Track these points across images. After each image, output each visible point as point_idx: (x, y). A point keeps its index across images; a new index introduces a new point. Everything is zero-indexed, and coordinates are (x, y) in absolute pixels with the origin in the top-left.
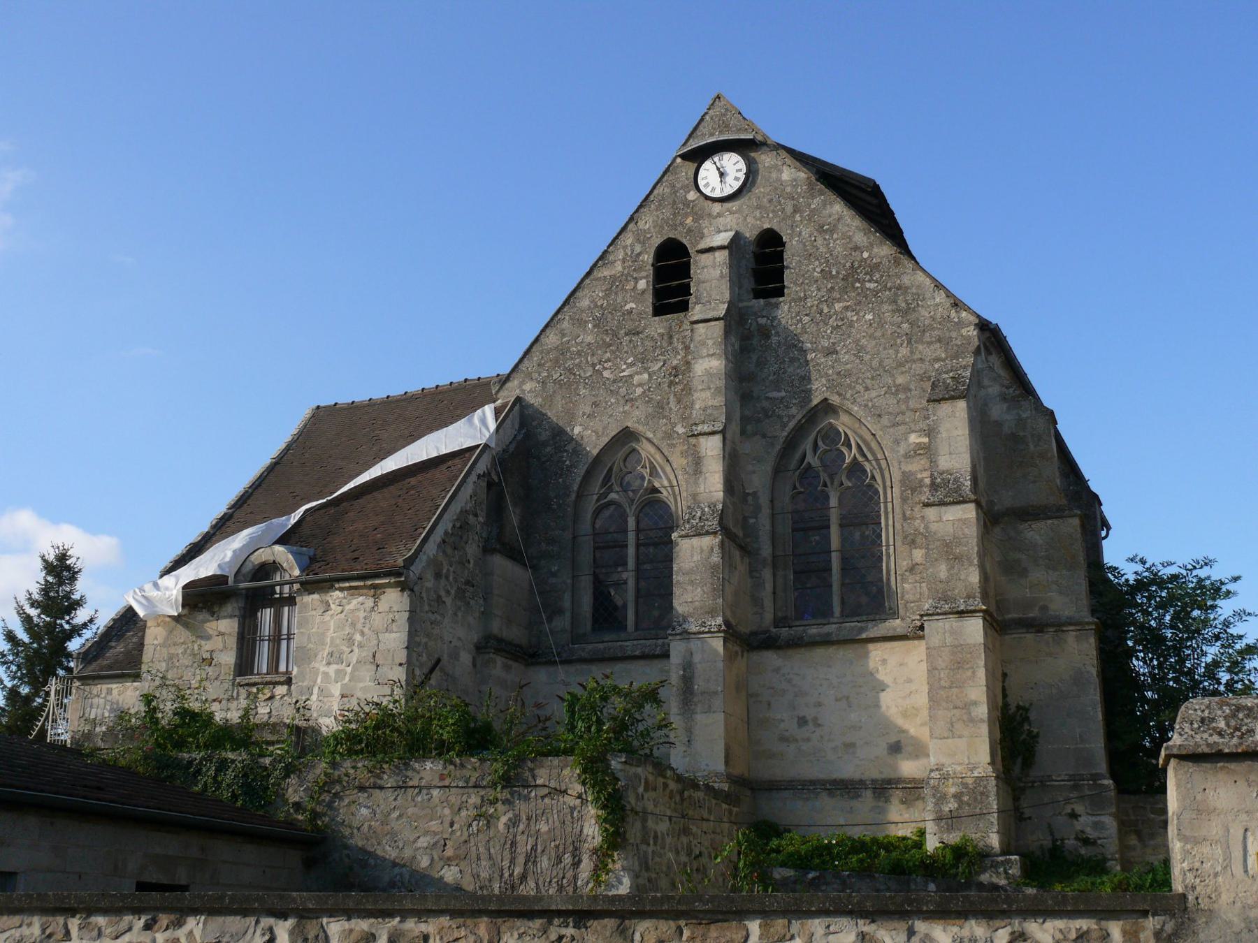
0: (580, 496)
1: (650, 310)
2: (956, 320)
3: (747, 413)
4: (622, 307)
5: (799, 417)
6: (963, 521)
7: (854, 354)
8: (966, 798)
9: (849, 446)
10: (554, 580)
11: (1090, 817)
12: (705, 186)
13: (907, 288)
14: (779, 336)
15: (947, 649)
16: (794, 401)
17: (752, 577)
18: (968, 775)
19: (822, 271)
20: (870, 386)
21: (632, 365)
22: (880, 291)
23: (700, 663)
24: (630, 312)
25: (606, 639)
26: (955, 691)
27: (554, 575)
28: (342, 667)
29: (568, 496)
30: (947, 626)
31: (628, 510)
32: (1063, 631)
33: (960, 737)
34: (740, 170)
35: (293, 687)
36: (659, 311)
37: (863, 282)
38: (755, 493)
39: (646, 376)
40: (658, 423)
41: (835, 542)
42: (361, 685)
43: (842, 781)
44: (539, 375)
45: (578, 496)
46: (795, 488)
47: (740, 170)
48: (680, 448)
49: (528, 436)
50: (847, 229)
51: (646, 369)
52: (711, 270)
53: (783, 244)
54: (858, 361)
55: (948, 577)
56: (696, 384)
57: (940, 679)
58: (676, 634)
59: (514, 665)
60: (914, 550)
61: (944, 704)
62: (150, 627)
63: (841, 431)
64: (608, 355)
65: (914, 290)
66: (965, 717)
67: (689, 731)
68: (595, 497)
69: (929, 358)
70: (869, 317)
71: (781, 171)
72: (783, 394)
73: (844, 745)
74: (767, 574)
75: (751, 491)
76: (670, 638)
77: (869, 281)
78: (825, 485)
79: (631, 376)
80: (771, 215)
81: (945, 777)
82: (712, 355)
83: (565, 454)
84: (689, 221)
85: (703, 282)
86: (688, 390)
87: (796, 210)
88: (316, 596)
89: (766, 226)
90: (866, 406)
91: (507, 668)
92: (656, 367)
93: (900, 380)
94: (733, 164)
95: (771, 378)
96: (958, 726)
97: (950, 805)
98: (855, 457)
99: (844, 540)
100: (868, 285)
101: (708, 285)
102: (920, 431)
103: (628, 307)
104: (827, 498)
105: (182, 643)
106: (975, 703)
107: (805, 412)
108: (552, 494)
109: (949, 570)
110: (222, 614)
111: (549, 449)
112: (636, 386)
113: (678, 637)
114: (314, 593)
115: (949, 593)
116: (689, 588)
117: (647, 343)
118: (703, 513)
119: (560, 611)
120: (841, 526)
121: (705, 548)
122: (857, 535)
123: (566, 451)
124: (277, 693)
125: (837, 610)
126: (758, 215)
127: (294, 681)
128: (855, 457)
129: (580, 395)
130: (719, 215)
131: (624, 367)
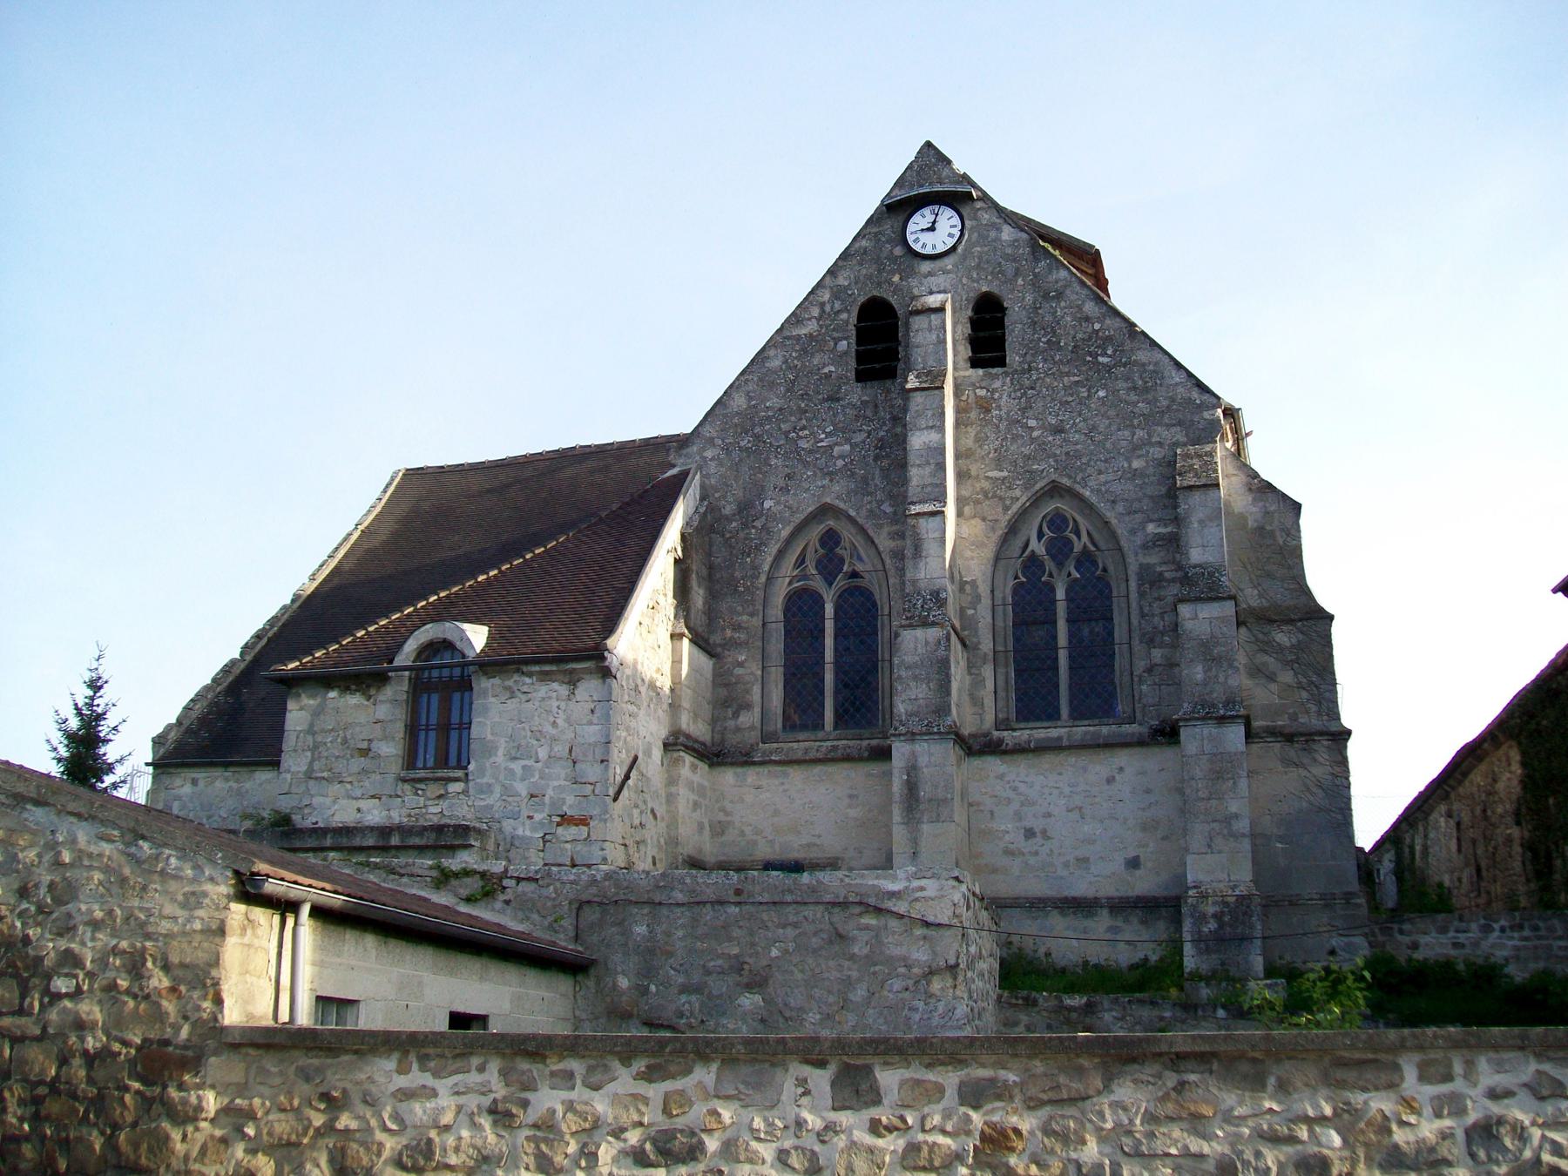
0: (770, 579)
1: (852, 375)
2: (1198, 402)
3: (964, 493)
4: (819, 369)
5: (1024, 499)
6: (1223, 619)
7: (1086, 434)
8: (1226, 919)
9: (1078, 535)
10: (739, 671)
11: (1342, 938)
12: (914, 241)
13: (1144, 365)
14: (1000, 410)
15: (1205, 757)
16: (1018, 483)
17: (970, 673)
18: (1230, 892)
19: (1049, 340)
20: (1103, 469)
21: (828, 435)
22: (1115, 366)
23: (926, 766)
24: (828, 376)
25: (800, 739)
26: (1214, 802)
27: (741, 665)
28: (530, 763)
29: (758, 578)
30: (1206, 731)
31: (825, 597)
32: (1314, 740)
33: (1220, 852)
34: (955, 226)
35: (471, 784)
36: (861, 377)
37: (1095, 356)
38: (974, 582)
39: (847, 447)
40: (862, 500)
41: (1062, 639)
42: (556, 783)
43: (1074, 899)
44: (723, 441)
45: (768, 579)
46: (1016, 577)
47: (955, 226)
48: (886, 529)
49: (711, 509)
50: (1076, 297)
51: (848, 441)
52: (928, 335)
53: (1003, 310)
54: (1089, 441)
55: (1205, 679)
56: (913, 458)
57: (1198, 791)
58: (900, 735)
59: (700, 764)
60: (1153, 650)
61: (1202, 817)
62: (290, 711)
63: (1068, 516)
64: (804, 422)
65: (1151, 367)
66: (1225, 832)
67: (915, 842)
68: (787, 580)
69: (1169, 442)
70: (1102, 394)
71: (999, 230)
72: (1005, 474)
73: (1077, 860)
74: (988, 672)
75: (969, 579)
76: (893, 739)
77: (1102, 355)
78: (1051, 575)
79: (831, 447)
80: (989, 277)
81: (1204, 896)
82: (932, 427)
83: (753, 531)
84: (896, 278)
85: (917, 347)
86: (903, 465)
87: (1017, 273)
88: (497, 681)
89: (984, 289)
90: (1099, 491)
91: (694, 768)
92: (859, 437)
93: (1136, 464)
94: (948, 222)
95: (991, 455)
96: (1218, 840)
97: (1210, 926)
98: (1085, 546)
99: (1071, 635)
100: (1101, 359)
101: (923, 349)
102: (1160, 520)
103: (826, 370)
104: (1053, 590)
105: (332, 730)
106: (1236, 816)
107: (1030, 495)
108: (737, 574)
109: (1205, 672)
110: (381, 697)
111: (734, 524)
112: (838, 458)
113: (902, 738)
114: (495, 677)
115: (1206, 697)
116: (913, 684)
117: (848, 410)
118: (925, 602)
119: (748, 706)
120: (1068, 621)
121: (931, 640)
122: (1086, 631)
123: (754, 527)
124: (450, 790)
125: (1065, 711)
126: (975, 276)
127: (470, 778)
128: (1085, 546)
129: (771, 465)
130: (930, 274)
131: (823, 436)
